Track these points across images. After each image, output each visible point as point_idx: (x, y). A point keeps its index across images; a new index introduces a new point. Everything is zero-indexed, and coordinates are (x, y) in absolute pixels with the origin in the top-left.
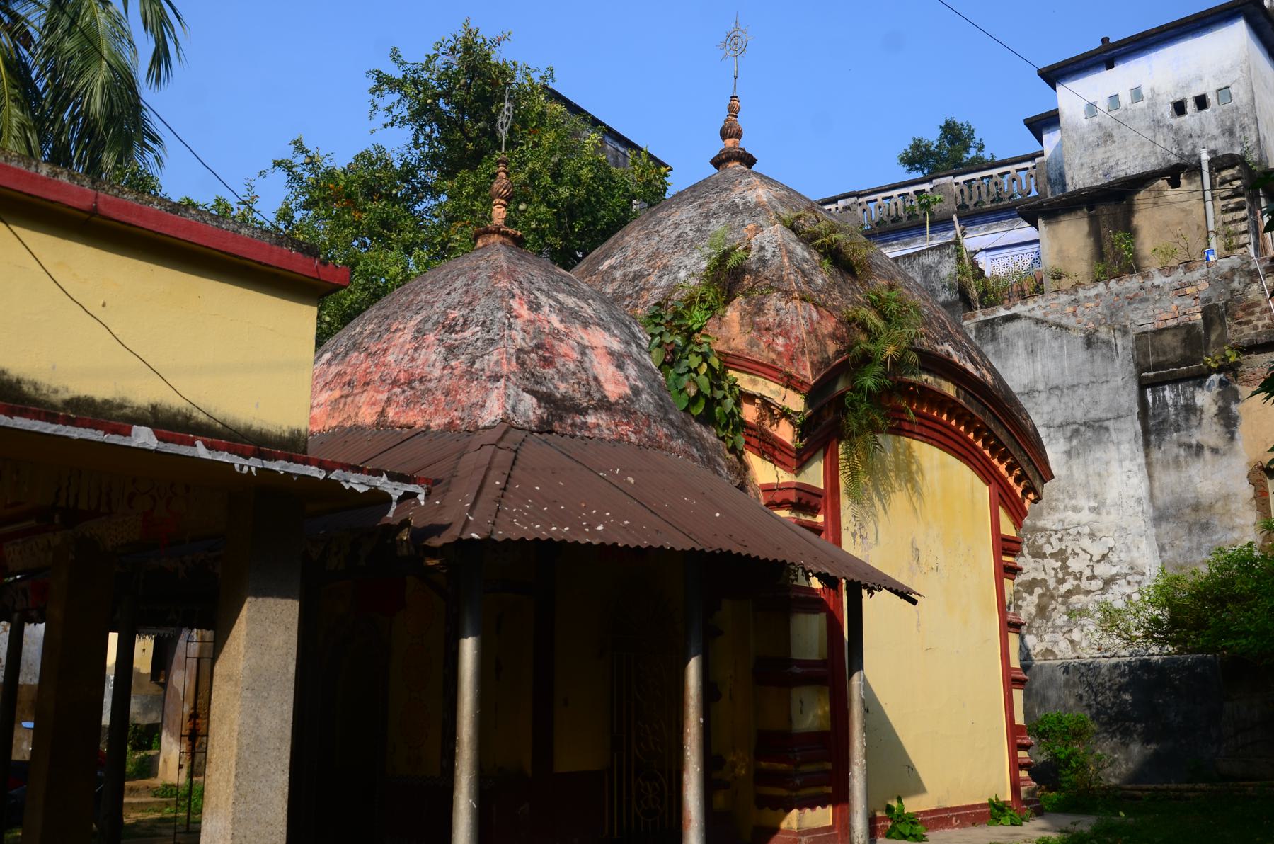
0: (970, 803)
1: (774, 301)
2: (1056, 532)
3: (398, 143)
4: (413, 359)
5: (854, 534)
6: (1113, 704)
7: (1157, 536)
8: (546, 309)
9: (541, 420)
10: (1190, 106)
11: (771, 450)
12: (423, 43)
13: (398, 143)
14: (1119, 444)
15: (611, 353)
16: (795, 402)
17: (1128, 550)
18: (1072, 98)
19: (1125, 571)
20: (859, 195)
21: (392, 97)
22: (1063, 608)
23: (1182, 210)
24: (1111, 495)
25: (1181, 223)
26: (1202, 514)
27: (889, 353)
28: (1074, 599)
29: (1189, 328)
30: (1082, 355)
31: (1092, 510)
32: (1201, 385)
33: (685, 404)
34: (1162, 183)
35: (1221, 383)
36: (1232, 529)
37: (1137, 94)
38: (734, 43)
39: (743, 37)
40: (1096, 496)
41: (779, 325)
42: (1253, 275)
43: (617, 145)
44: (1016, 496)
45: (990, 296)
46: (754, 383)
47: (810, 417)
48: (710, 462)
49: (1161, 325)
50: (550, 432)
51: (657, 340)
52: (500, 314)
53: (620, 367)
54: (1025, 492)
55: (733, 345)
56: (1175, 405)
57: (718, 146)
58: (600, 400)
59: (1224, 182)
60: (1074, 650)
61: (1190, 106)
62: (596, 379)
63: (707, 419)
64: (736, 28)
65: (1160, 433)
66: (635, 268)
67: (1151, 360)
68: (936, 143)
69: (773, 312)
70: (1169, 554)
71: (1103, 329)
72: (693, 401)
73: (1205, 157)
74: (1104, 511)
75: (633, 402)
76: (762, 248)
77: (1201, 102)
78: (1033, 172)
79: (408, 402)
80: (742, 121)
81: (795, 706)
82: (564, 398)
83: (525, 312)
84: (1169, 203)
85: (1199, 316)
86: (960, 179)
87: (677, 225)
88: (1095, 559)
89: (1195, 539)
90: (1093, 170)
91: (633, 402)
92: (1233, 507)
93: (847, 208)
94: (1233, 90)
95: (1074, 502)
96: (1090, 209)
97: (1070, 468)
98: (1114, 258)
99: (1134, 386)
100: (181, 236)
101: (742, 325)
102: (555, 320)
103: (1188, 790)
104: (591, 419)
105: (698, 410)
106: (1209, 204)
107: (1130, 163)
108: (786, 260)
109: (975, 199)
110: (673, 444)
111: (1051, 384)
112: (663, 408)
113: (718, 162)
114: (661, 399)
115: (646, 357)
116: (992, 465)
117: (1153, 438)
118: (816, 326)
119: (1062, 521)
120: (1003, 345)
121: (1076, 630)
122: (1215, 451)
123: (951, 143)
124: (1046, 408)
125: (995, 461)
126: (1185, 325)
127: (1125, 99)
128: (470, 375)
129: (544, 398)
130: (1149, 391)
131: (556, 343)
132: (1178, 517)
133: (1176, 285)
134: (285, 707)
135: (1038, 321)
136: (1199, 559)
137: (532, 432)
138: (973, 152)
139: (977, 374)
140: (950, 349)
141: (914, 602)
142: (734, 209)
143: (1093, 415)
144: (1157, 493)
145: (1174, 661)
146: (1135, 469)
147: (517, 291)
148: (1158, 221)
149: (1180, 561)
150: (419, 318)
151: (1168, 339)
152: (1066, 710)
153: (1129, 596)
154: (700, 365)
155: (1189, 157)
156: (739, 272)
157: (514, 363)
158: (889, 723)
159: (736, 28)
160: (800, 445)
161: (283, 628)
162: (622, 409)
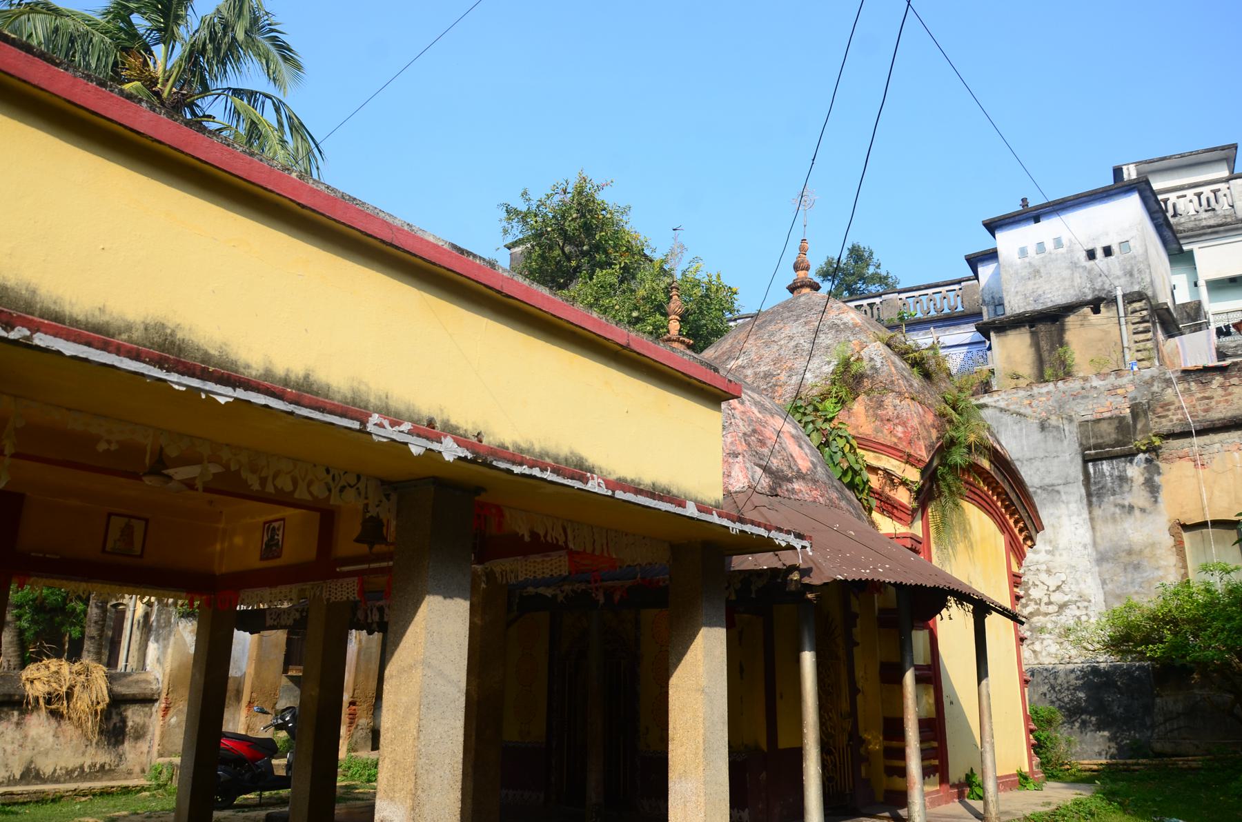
10: (1099, 253)
11: (890, 508)
14: (1068, 503)
15: (793, 436)
16: (913, 475)
17: (1077, 583)
18: (1007, 241)
19: (1075, 598)
23: (1103, 331)
24: (1063, 542)
25: (1101, 340)
26: (1134, 557)
29: (1121, 419)
30: (1037, 436)
31: (1048, 552)
32: (1131, 462)
34: (1087, 310)
35: (1147, 461)
36: (1158, 569)
37: (1058, 243)
41: (898, 417)
42: (1168, 382)
46: (879, 459)
48: (859, 518)
49: (1099, 416)
51: (811, 426)
54: (1025, 540)
55: (861, 430)
56: (1111, 475)
57: (791, 276)
59: (1134, 311)
60: (1036, 657)
61: (1099, 253)
65: (1100, 496)
66: (763, 368)
67: (1092, 441)
69: (891, 408)
70: (1110, 586)
73: (1119, 293)
74: (1057, 553)
76: (871, 359)
77: (1108, 251)
78: (960, 293)
84: (1092, 325)
85: (1128, 411)
87: (791, 338)
89: (1130, 576)
90: (1026, 297)
92: (1158, 552)
94: (1131, 244)
96: (1031, 327)
98: (1051, 365)
99: (1079, 460)
104: (796, 486)
106: (1124, 328)
107: (1054, 294)
113: (792, 289)
117: (1094, 499)
121: (1037, 643)
122: (1143, 510)
123: (856, 262)
126: (1118, 417)
127: (1049, 246)
130: (1090, 464)
132: (1115, 559)
133: (1109, 387)
135: (1002, 410)
136: (1133, 590)
138: (871, 270)
143: (1047, 481)
144: (1099, 540)
145: (1116, 667)
148: (1082, 335)
149: (1118, 592)
151: (1104, 426)
153: (1079, 618)
155: (1100, 290)
156: (859, 378)
160: (915, 505)
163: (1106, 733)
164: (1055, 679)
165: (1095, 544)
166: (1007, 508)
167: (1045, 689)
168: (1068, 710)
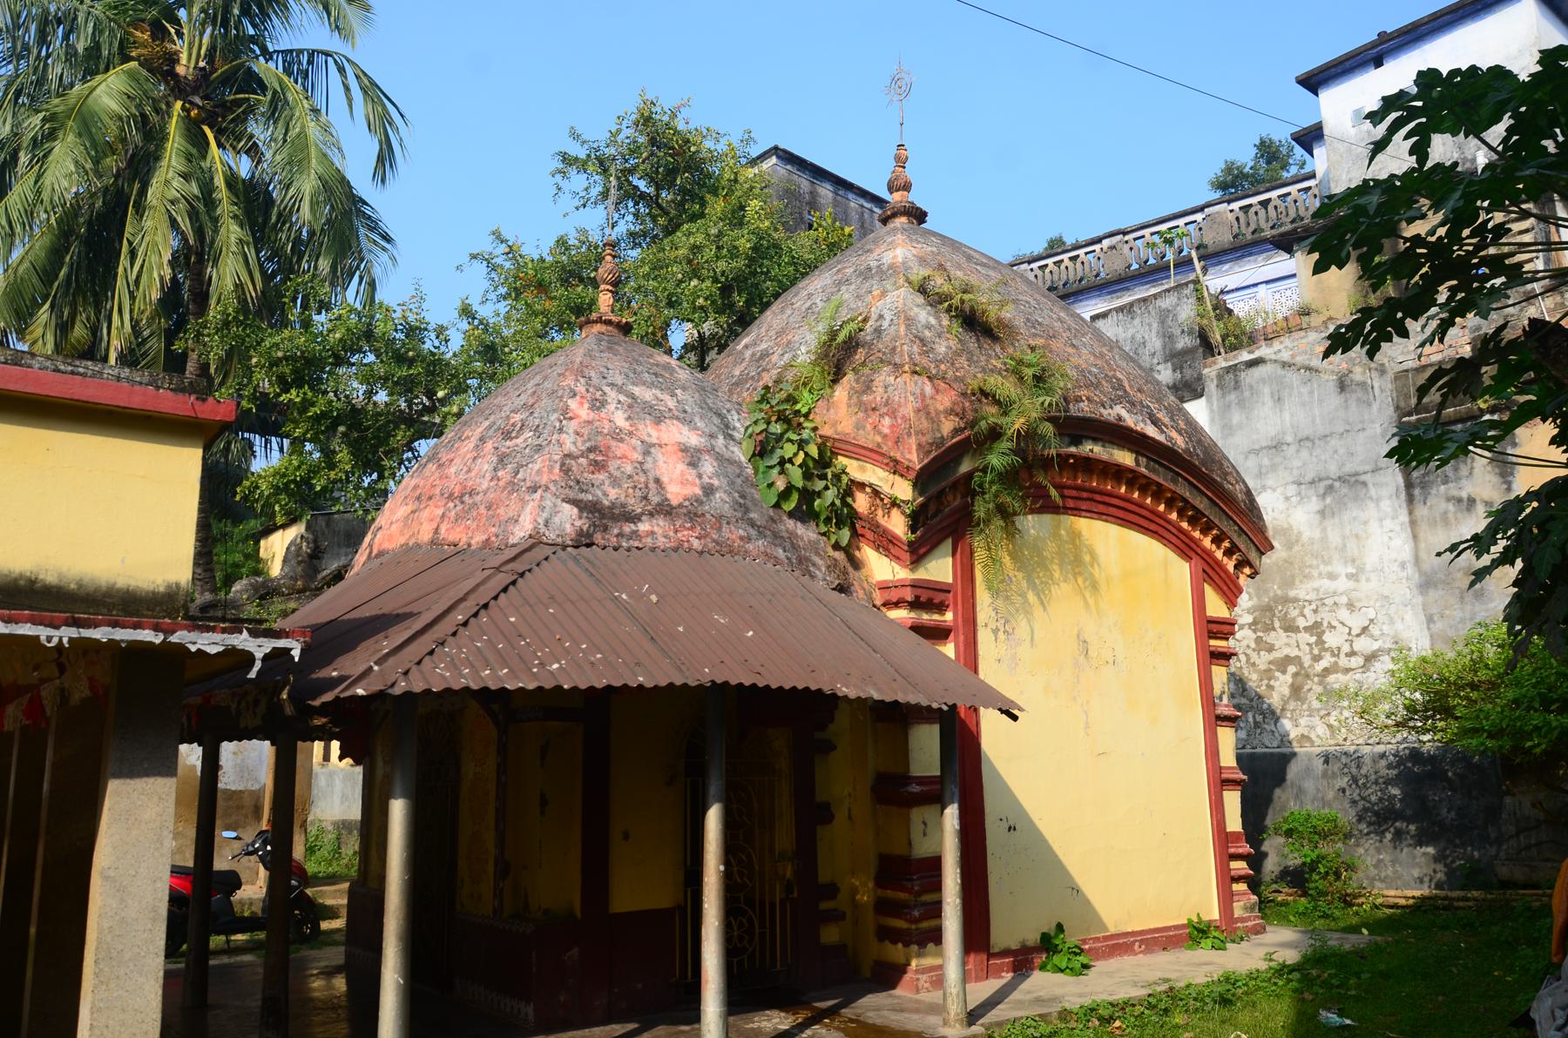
0: (1152, 926)
1: (884, 377)
2: (1310, 602)
3: (596, 222)
4: (469, 471)
5: (995, 631)
6: (1381, 799)
7: (1424, 605)
8: (612, 407)
9: (580, 533)
11: (885, 542)
12: (604, 120)
13: (596, 222)
14: (1378, 500)
15: (685, 449)
16: (903, 490)
17: (1392, 621)
20: (1125, 233)
21: (578, 181)
22: (1319, 689)
24: (1371, 560)
27: (1017, 426)
28: (1332, 678)
30: (1335, 400)
31: (1350, 576)
33: (774, 500)
38: (899, 86)
39: (907, 80)
40: (1353, 561)
41: (887, 404)
43: (862, 201)
44: (1226, 571)
45: (1241, 337)
46: (863, 469)
47: (923, 506)
48: (802, 564)
50: (588, 545)
52: (554, 417)
53: (693, 464)
55: (839, 428)
58: (658, 504)
62: (657, 481)
63: (805, 513)
64: (900, 71)
66: (764, 346)
68: (1251, 164)
69: (881, 390)
70: (1439, 626)
71: (1358, 370)
72: (785, 495)
74: (1363, 578)
75: (701, 503)
76: (881, 317)
79: (458, 518)
80: (910, 173)
81: (916, 828)
82: (613, 505)
83: (584, 413)
85: (1468, 348)
86: (1236, 206)
87: (810, 295)
88: (1354, 632)
89: (1468, 607)
91: (701, 503)
93: (1112, 248)
95: (1329, 568)
97: (1324, 530)
100: (12, 387)
101: (849, 406)
102: (620, 419)
103: (1459, 899)
104: (644, 527)
105: (790, 505)
108: (902, 329)
109: (1253, 227)
110: (750, 547)
111: (1300, 435)
112: (743, 507)
114: (743, 497)
115: (735, 449)
116: (1192, 539)
117: (1417, 492)
118: (928, 401)
119: (1317, 590)
120: (1247, 394)
123: (1269, 163)
124: (1296, 463)
125: (1197, 534)
128: (512, 486)
129: (590, 509)
131: (613, 443)
134: (159, 885)
135: (1285, 365)
137: (564, 547)
139: (1161, 438)
140: (1124, 413)
141: (1015, 718)
142: (866, 274)
143: (1349, 468)
146: (1398, 528)
147: (581, 388)
150: (487, 423)
152: (1325, 804)
154: (796, 455)
157: (557, 470)
158: (1046, 841)
159: (900, 71)
160: (912, 537)
161: (156, 799)
162: (691, 513)
163: (1431, 850)
164: (1359, 767)
165: (1417, 560)
166: (1193, 521)
167: (1343, 782)
168: (1376, 814)
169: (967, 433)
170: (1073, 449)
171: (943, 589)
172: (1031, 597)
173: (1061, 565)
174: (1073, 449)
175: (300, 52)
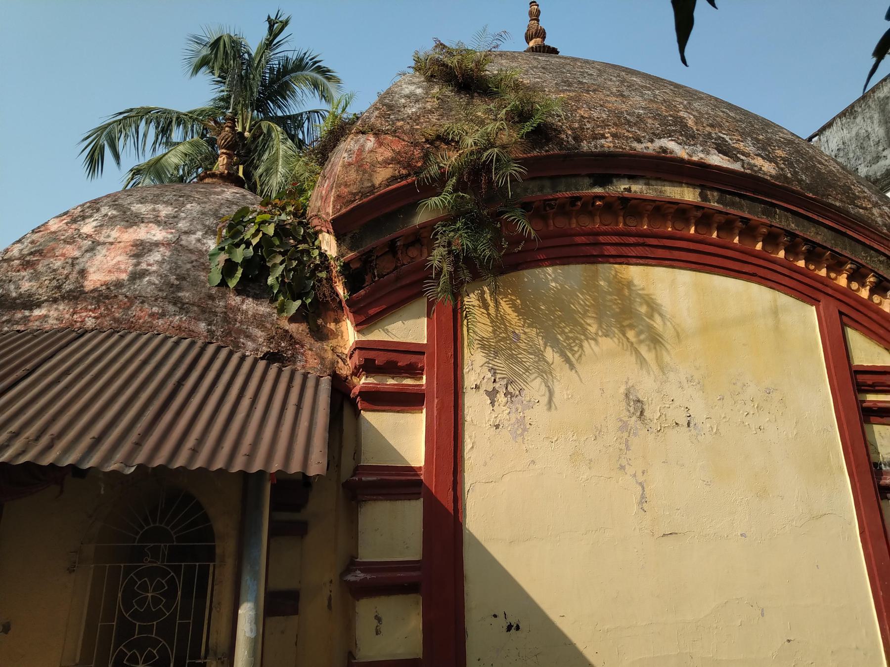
5: (492, 394)
80: (543, 23)
139: (737, 166)
169: (409, 180)
170: (598, 190)
171: (415, 350)
172: (550, 354)
173: (599, 320)
174: (598, 190)
175: (301, 114)
